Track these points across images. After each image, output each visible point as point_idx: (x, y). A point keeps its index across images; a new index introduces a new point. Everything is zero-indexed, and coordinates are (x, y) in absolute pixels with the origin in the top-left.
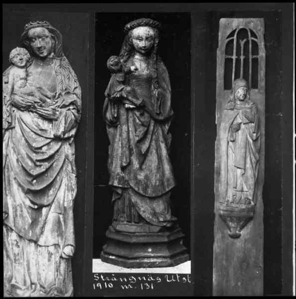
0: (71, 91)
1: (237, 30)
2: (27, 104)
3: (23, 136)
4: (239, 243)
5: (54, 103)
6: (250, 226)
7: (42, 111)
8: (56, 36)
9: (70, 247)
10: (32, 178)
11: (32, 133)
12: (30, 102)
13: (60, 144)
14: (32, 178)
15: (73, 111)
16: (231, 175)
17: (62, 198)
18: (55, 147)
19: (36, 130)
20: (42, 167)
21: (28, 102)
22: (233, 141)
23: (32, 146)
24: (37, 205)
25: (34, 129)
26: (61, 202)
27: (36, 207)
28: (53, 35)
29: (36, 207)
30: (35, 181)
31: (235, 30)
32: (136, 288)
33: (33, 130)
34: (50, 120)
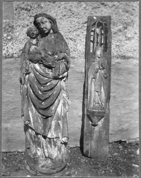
0: (63, 51)
1: (97, 23)
2: (37, 59)
3: (36, 77)
4: (96, 129)
5: (53, 58)
6: (103, 120)
7: (46, 63)
8: (52, 21)
9: (66, 138)
10: (41, 101)
11: (41, 75)
12: (39, 58)
13: (58, 80)
14: (41, 101)
15: (65, 62)
16: (93, 94)
17: (60, 111)
18: (54, 82)
19: (43, 73)
20: (47, 95)
21: (37, 58)
22: (94, 78)
23: (41, 83)
24: (45, 116)
25: (42, 73)
26: (60, 114)
27: (45, 117)
28: (50, 21)
29: (45, 117)
30: (43, 103)
31: (96, 22)
32: (126, 152)
33: (41, 74)
34: (50, 67)
